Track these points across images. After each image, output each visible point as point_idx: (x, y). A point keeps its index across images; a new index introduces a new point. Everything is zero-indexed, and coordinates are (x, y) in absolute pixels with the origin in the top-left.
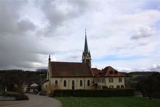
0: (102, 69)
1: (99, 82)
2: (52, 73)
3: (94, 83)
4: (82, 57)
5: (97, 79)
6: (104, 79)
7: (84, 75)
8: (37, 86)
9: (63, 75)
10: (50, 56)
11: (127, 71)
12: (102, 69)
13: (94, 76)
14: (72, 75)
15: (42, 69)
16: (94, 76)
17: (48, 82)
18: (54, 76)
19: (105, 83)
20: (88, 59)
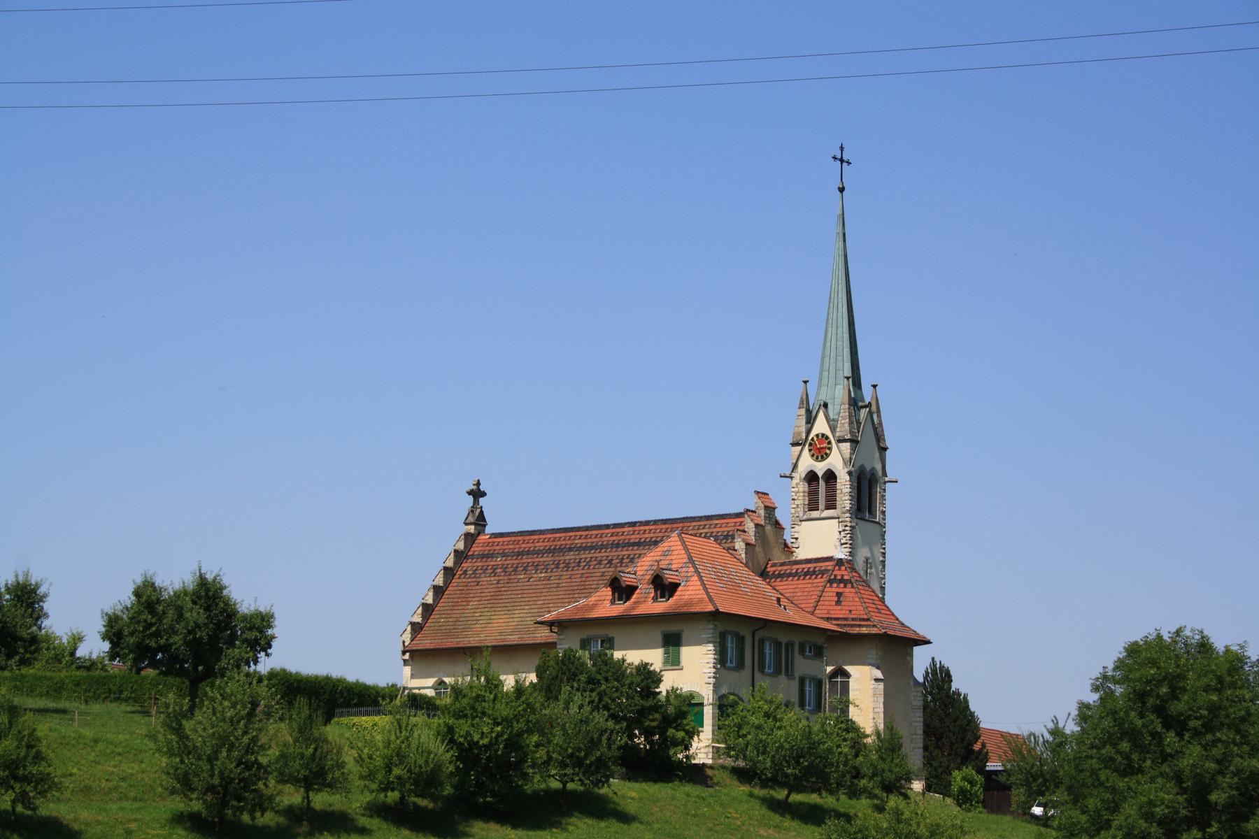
10: (477, 494)
20: (820, 468)
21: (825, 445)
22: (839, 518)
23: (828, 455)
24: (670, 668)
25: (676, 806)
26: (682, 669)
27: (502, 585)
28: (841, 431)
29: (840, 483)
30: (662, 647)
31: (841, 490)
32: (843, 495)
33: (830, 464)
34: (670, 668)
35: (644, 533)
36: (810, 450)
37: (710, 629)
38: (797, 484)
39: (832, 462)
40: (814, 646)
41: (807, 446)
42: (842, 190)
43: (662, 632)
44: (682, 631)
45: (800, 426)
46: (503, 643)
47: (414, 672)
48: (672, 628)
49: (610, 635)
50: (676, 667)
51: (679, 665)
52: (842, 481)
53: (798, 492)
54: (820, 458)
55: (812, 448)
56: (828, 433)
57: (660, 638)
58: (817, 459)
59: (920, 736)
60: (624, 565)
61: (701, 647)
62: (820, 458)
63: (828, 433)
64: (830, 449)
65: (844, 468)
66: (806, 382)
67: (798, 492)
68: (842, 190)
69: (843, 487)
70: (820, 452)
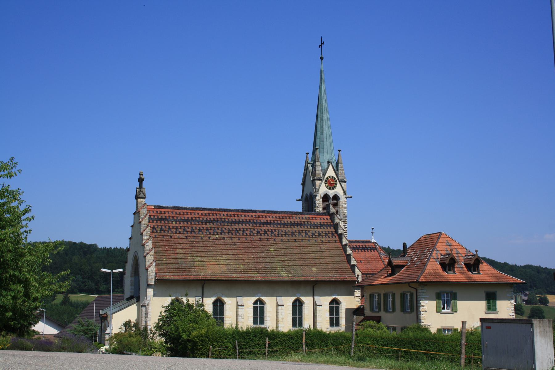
0: (405, 245)
1: (386, 310)
2: (154, 264)
3: (364, 315)
4: (303, 184)
5: (394, 295)
6: (412, 295)
7: (314, 274)
8: (136, 299)
9: (208, 275)
10: (141, 180)
11: (125, 284)
12: (405, 245)
13: (360, 279)
14: (255, 275)
15: (327, 364)
16: (360, 279)
17: (320, 181)
18: (168, 275)
19: (414, 314)
20: (331, 193)
21: (334, 182)
22: (342, 219)
23: (335, 187)
24: (491, 312)
25: (171, 362)
26: (497, 313)
27: (212, 240)
28: (341, 177)
29: (342, 202)
30: (485, 300)
31: (343, 205)
32: (343, 208)
33: (336, 192)
34: (491, 312)
35: (165, 213)
36: (326, 184)
37: (512, 291)
38: (319, 199)
39: (337, 191)
40: (450, 293)
41: (324, 181)
42: (322, 59)
43: (485, 291)
44: (496, 291)
45: (319, 171)
46: (231, 279)
47: (155, 293)
48: (491, 290)
49: (454, 291)
50: (495, 312)
51: (496, 311)
52: (343, 201)
53: (320, 204)
54: (331, 188)
55: (326, 182)
56: (335, 176)
57: (484, 295)
58: (330, 189)
59: (240, 320)
60: (198, 228)
61: (507, 301)
62: (331, 188)
63: (335, 176)
64: (336, 184)
65: (343, 195)
66: (339, 151)
67: (320, 204)
68: (322, 59)
69: (343, 204)
70: (331, 185)
